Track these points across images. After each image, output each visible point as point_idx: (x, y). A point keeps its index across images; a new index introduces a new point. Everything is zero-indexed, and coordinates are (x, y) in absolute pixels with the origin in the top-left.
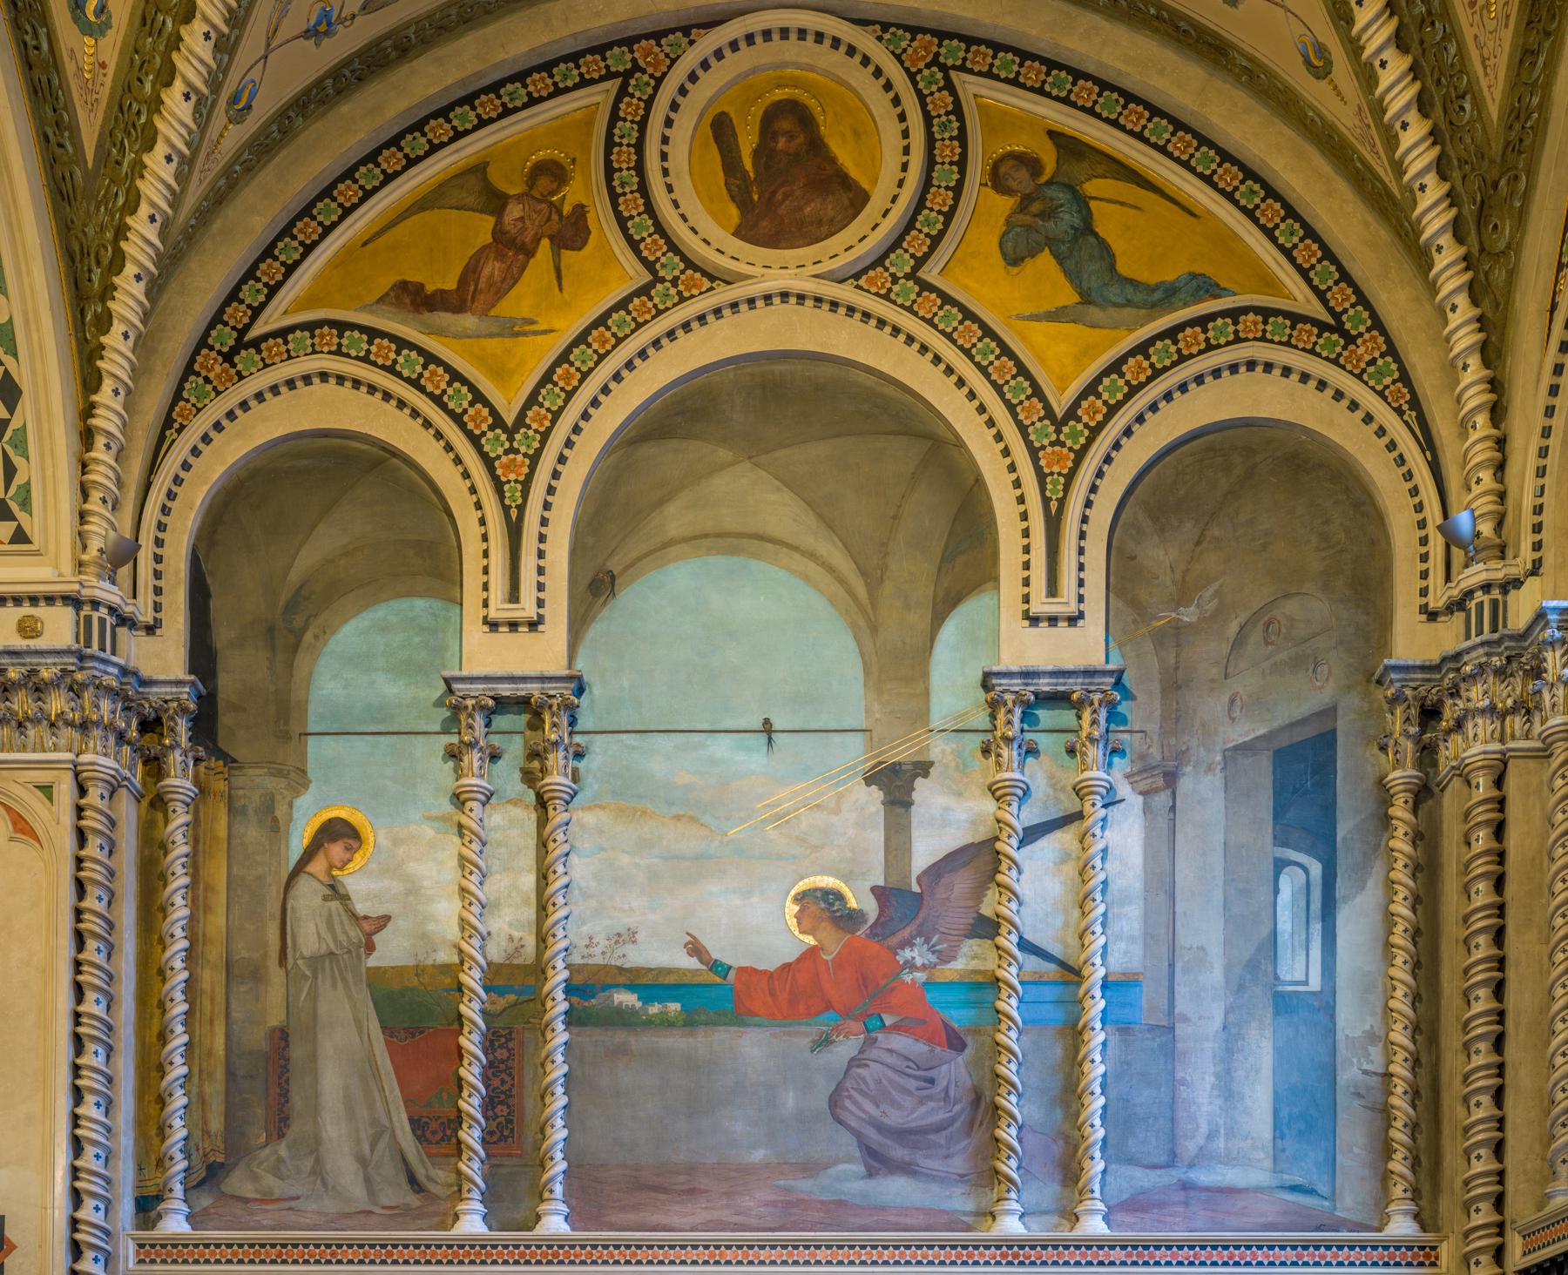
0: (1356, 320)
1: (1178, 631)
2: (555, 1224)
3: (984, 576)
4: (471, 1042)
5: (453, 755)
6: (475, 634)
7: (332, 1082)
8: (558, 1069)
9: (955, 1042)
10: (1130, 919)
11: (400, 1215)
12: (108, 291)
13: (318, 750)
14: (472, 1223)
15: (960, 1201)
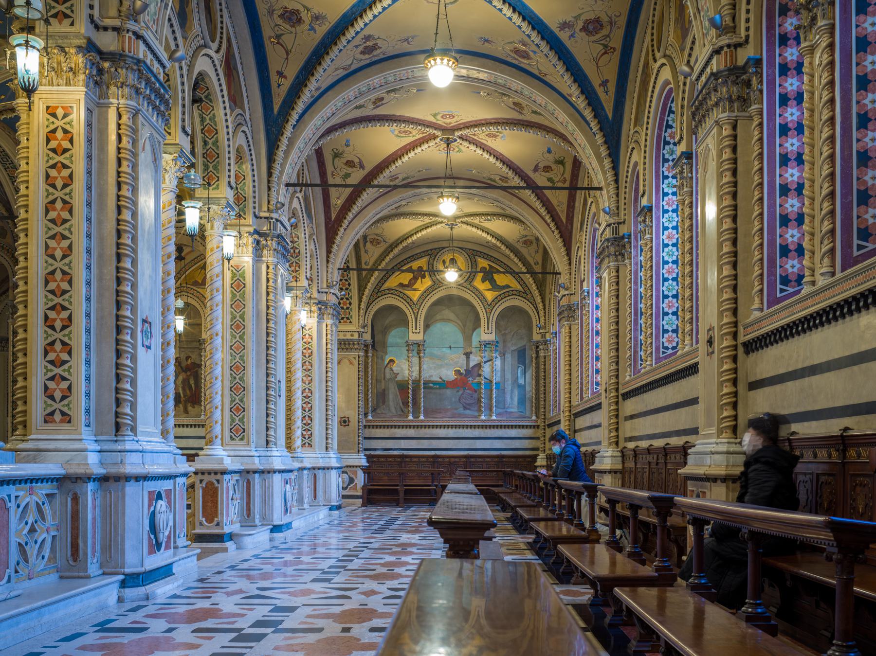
0: (528, 292)
1: (505, 334)
2: (422, 417)
3: (479, 326)
4: (410, 391)
5: (408, 350)
6: (411, 333)
7: (391, 397)
8: (422, 395)
9: (475, 391)
10: (499, 374)
11: (400, 416)
12: (364, 291)
13: (389, 349)
14: (411, 417)
15: (476, 414)
